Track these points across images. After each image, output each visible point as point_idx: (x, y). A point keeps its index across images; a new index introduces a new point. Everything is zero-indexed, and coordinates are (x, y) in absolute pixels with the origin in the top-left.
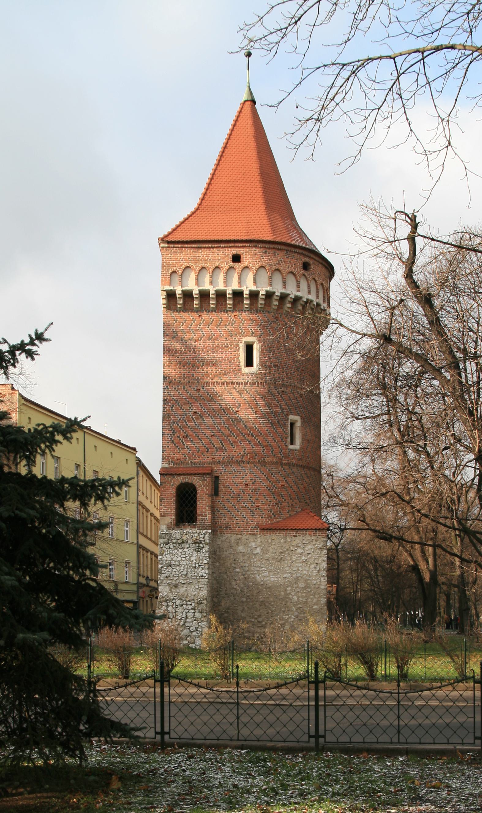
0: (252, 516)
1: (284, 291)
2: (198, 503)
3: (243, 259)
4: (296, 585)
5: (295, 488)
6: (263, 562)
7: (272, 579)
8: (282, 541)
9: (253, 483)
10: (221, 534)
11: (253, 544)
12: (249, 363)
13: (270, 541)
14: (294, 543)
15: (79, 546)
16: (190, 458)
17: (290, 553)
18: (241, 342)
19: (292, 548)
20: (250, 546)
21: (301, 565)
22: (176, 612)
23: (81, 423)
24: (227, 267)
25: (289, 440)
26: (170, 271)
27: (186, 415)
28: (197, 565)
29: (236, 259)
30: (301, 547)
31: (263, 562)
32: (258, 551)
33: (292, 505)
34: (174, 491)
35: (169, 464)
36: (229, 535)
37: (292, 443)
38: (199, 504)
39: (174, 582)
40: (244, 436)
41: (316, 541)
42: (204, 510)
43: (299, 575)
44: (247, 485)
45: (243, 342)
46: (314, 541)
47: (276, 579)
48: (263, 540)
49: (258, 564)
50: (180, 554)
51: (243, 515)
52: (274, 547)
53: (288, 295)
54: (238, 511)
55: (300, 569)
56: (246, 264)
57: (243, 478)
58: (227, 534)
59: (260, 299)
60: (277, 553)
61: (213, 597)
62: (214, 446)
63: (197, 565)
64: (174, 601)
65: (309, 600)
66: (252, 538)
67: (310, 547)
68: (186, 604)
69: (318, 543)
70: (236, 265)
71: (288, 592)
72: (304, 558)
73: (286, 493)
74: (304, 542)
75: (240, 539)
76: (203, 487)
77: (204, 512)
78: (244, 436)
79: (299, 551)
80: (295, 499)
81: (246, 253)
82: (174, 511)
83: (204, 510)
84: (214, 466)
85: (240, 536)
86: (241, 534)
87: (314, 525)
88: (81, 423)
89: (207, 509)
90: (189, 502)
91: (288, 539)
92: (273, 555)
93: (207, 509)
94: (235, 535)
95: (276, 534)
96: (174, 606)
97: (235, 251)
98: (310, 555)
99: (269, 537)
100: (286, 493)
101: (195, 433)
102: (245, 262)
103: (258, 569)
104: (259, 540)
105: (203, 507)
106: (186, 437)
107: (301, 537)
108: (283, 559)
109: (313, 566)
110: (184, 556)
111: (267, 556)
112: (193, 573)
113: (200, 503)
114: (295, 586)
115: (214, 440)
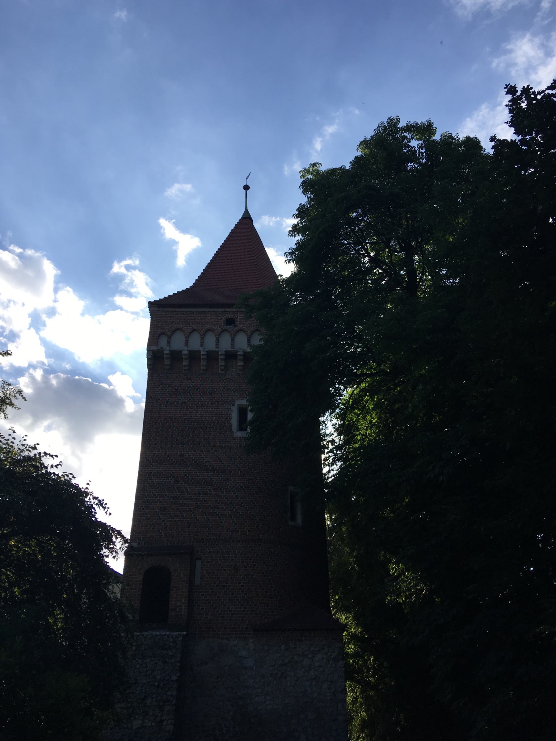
0: (243, 611)
8: (283, 647)
9: (245, 567)
12: (241, 428)
18: (234, 405)
23: (128, 536)
24: (220, 330)
27: (165, 484)
30: (309, 656)
35: (139, 544)
37: (293, 518)
45: (236, 405)
51: (231, 611)
56: (241, 327)
57: (233, 560)
61: (355, 164)
63: (162, 684)
74: (312, 649)
88: (128, 536)
89: (183, 600)
93: (183, 600)
101: (175, 504)
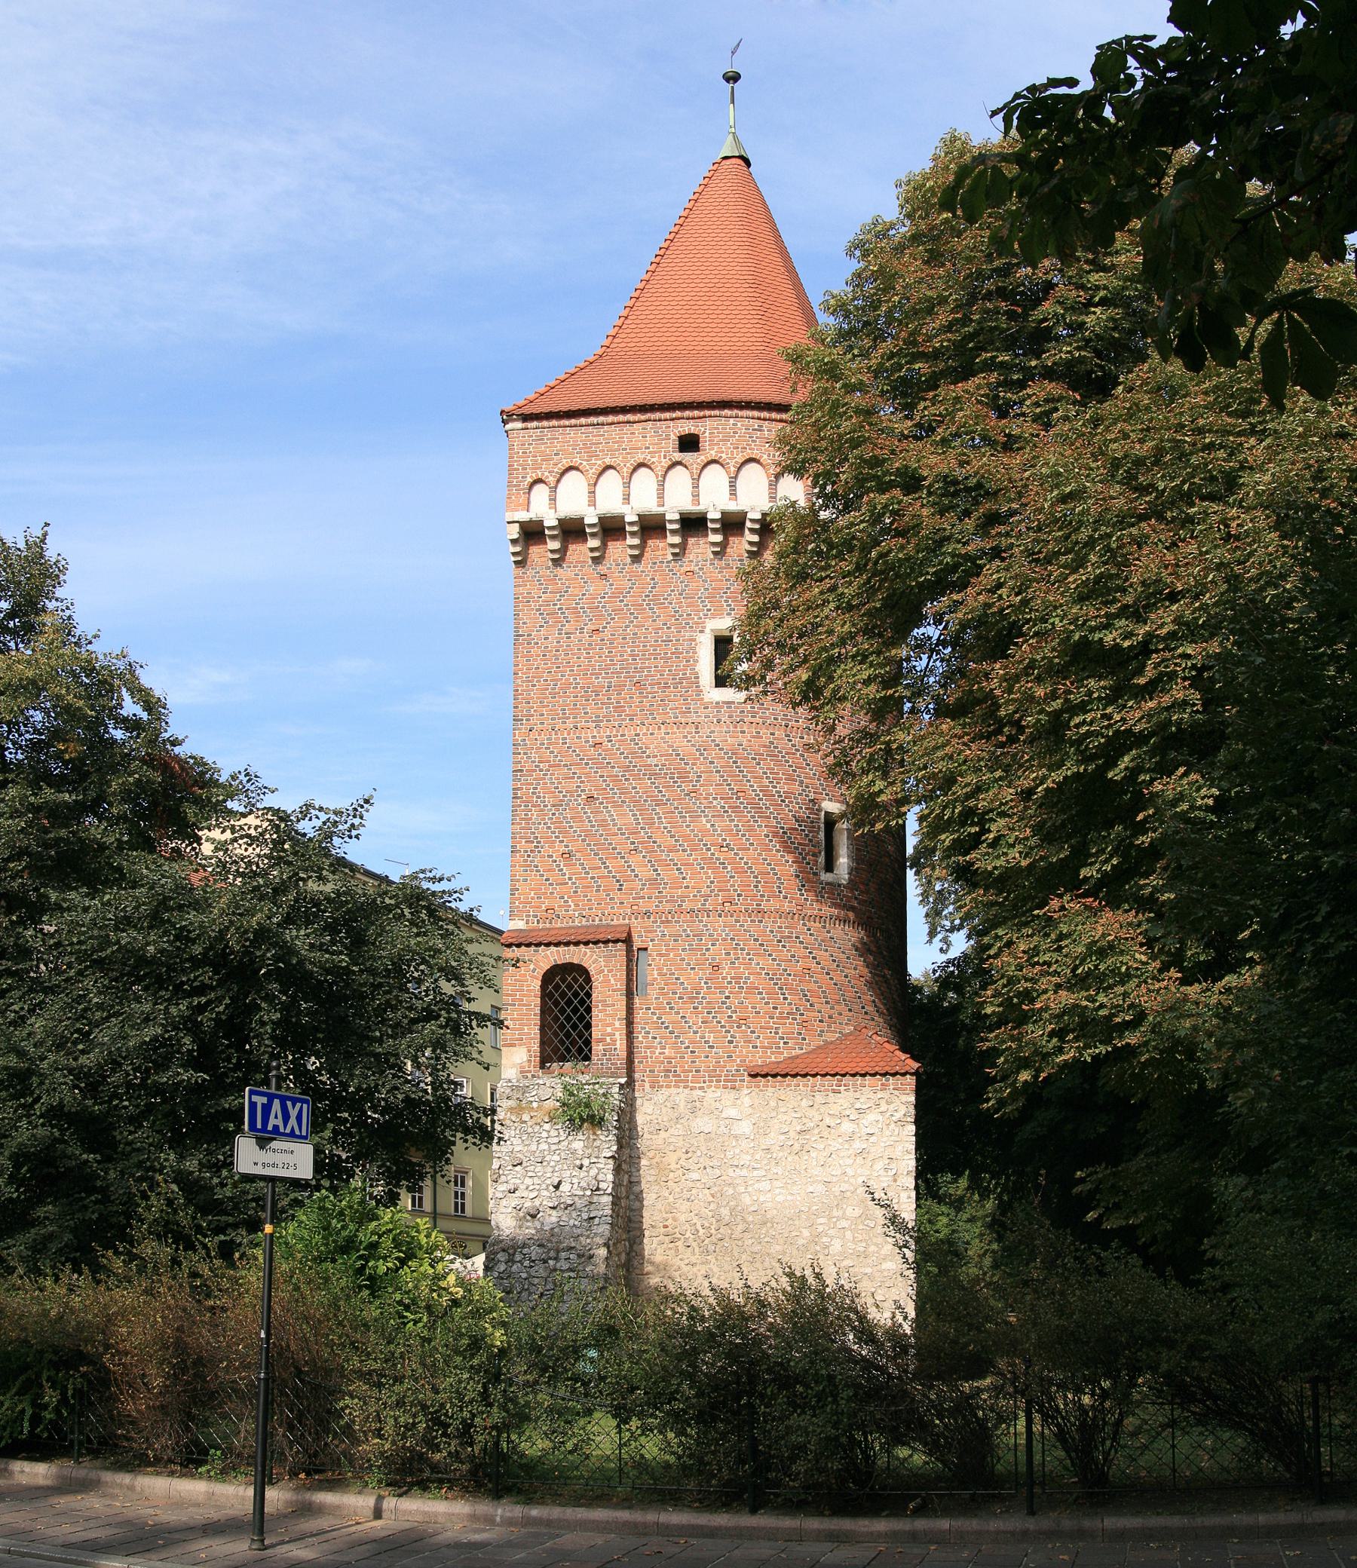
0: (731, 1042)
1: (732, 507)
2: (595, 1012)
3: (704, 444)
4: (840, 1213)
5: (838, 977)
6: (758, 1157)
7: (780, 1198)
8: (805, 1103)
10: (652, 1087)
11: (732, 1112)
13: (773, 1104)
14: (835, 1109)
15: (1087, 1523)
16: (577, 905)
17: (825, 1134)
19: (828, 1121)
20: (724, 1115)
21: (849, 1161)
22: (530, 1276)
24: (666, 463)
25: (822, 859)
26: (529, 480)
28: (586, 1162)
29: (689, 443)
31: (758, 1157)
32: (745, 1127)
33: (830, 1017)
34: (537, 984)
36: (673, 1090)
37: (829, 867)
38: (598, 1016)
39: (528, 1204)
40: (709, 849)
41: (888, 1103)
42: (609, 1030)
43: (845, 1187)
44: (716, 967)
45: (707, 630)
46: (883, 1103)
47: (789, 1198)
48: (757, 1102)
49: (745, 1159)
50: (545, 1135)
52: (785, 1117)
53: (743, 515)
54: (696, 1032)
55: (850, 1172)
56: (713, 454)
57: (708, 950)
58: (668, 1087)
59: (747, 532)
60: (792, 1134)
62: (636, 876)
64: (525, 1251)
65: (872, 1248)
66: (729, 1096)
67: (872, 1116)
68: (556, 1259)
69: (891, 1107)
70: (688, 457)
71: (821, 1229)
72: (858, 1145)
73: (814, 987)
74: (858, 1106)
75: (701, 1100)
76: (604, 968)
77: (609, 1035)
78: (709, 849)
79: (847, 1127)
80: (838, 1002)
81: (707, 427)
82: (535, 1031)
83: (609, 1030)
84: (634, 922)
85: (700, 1093)
86: (701, 1088)
87: (872, 1064)
90: (575, 1010)
91: (819, 1098)
92: (783, 1137)
94: (687, 1091)
95: (789, 1085)
96: (526, 1263)
97: (687, 428)
98: (872, 1139)
99: (772, 1090)
100: (814, 987)
102: (708, 451)
103: (744, 1172)
104: (747, 1101)
105: (606, 1024)
106: (568, 855)
107: (851, 1093)
108: (807, 1147)
109: (879, 1165)
110: (556, 1140)
111: (766, 1142)
112: (575, 1181)
113: (600, 1011)
114: (835, 1213)
115: (634, 860)
